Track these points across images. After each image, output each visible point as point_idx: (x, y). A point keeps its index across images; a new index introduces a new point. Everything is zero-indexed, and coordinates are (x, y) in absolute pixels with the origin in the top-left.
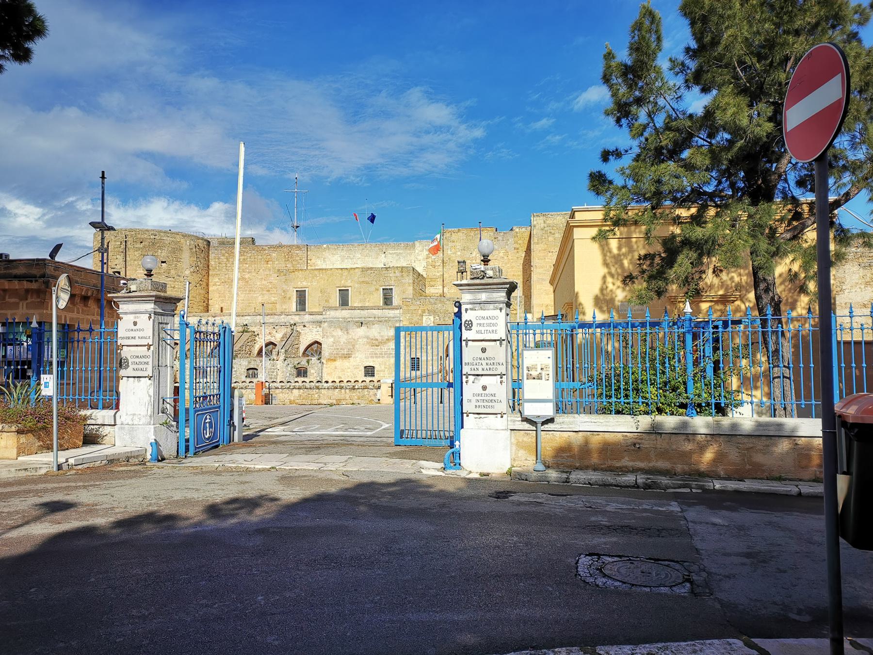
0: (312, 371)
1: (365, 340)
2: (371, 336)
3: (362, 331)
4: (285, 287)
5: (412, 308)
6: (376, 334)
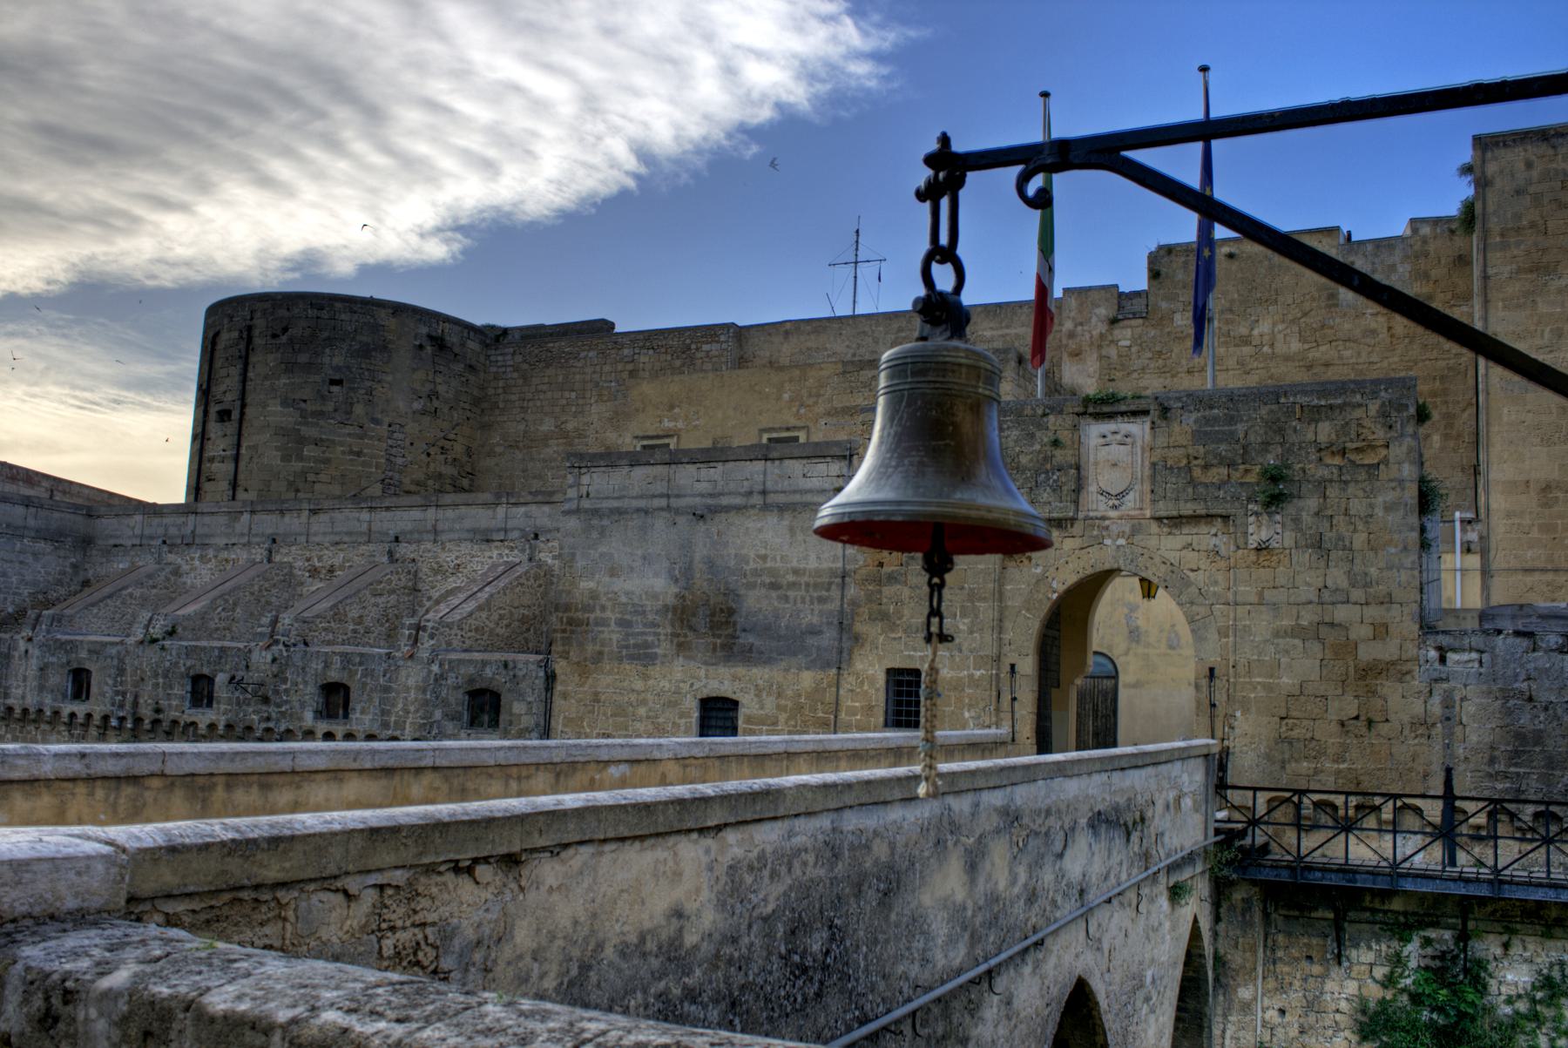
0: (518, 708)
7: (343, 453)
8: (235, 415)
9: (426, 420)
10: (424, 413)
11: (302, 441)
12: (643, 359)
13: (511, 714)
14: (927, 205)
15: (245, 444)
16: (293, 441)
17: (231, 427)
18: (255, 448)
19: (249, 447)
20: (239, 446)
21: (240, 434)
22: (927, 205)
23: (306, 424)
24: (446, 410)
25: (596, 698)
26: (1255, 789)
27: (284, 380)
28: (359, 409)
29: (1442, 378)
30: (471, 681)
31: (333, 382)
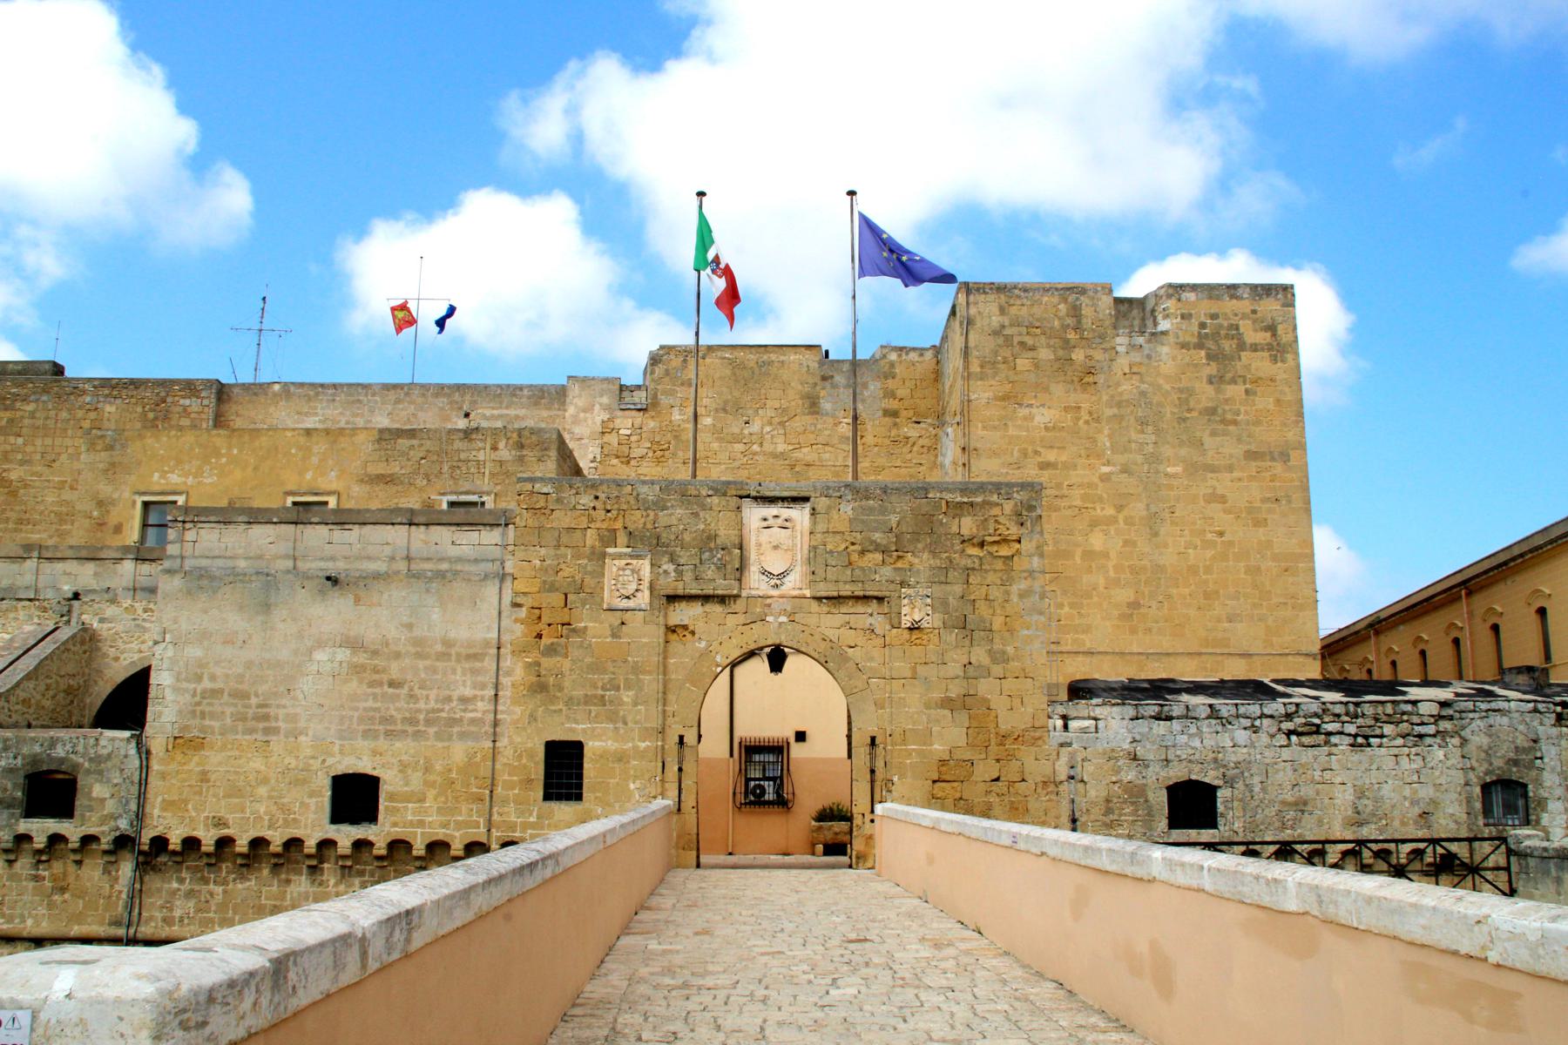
0: (99, 790)
1: (343, 654)
2: (371, 635)
3: (333, 613)
4: (105, 489)
5: (562, 519)
6: (392, 632)
12: (109, 408)
13: (91, 799)
25: (204, 777)
30: (35, 759)
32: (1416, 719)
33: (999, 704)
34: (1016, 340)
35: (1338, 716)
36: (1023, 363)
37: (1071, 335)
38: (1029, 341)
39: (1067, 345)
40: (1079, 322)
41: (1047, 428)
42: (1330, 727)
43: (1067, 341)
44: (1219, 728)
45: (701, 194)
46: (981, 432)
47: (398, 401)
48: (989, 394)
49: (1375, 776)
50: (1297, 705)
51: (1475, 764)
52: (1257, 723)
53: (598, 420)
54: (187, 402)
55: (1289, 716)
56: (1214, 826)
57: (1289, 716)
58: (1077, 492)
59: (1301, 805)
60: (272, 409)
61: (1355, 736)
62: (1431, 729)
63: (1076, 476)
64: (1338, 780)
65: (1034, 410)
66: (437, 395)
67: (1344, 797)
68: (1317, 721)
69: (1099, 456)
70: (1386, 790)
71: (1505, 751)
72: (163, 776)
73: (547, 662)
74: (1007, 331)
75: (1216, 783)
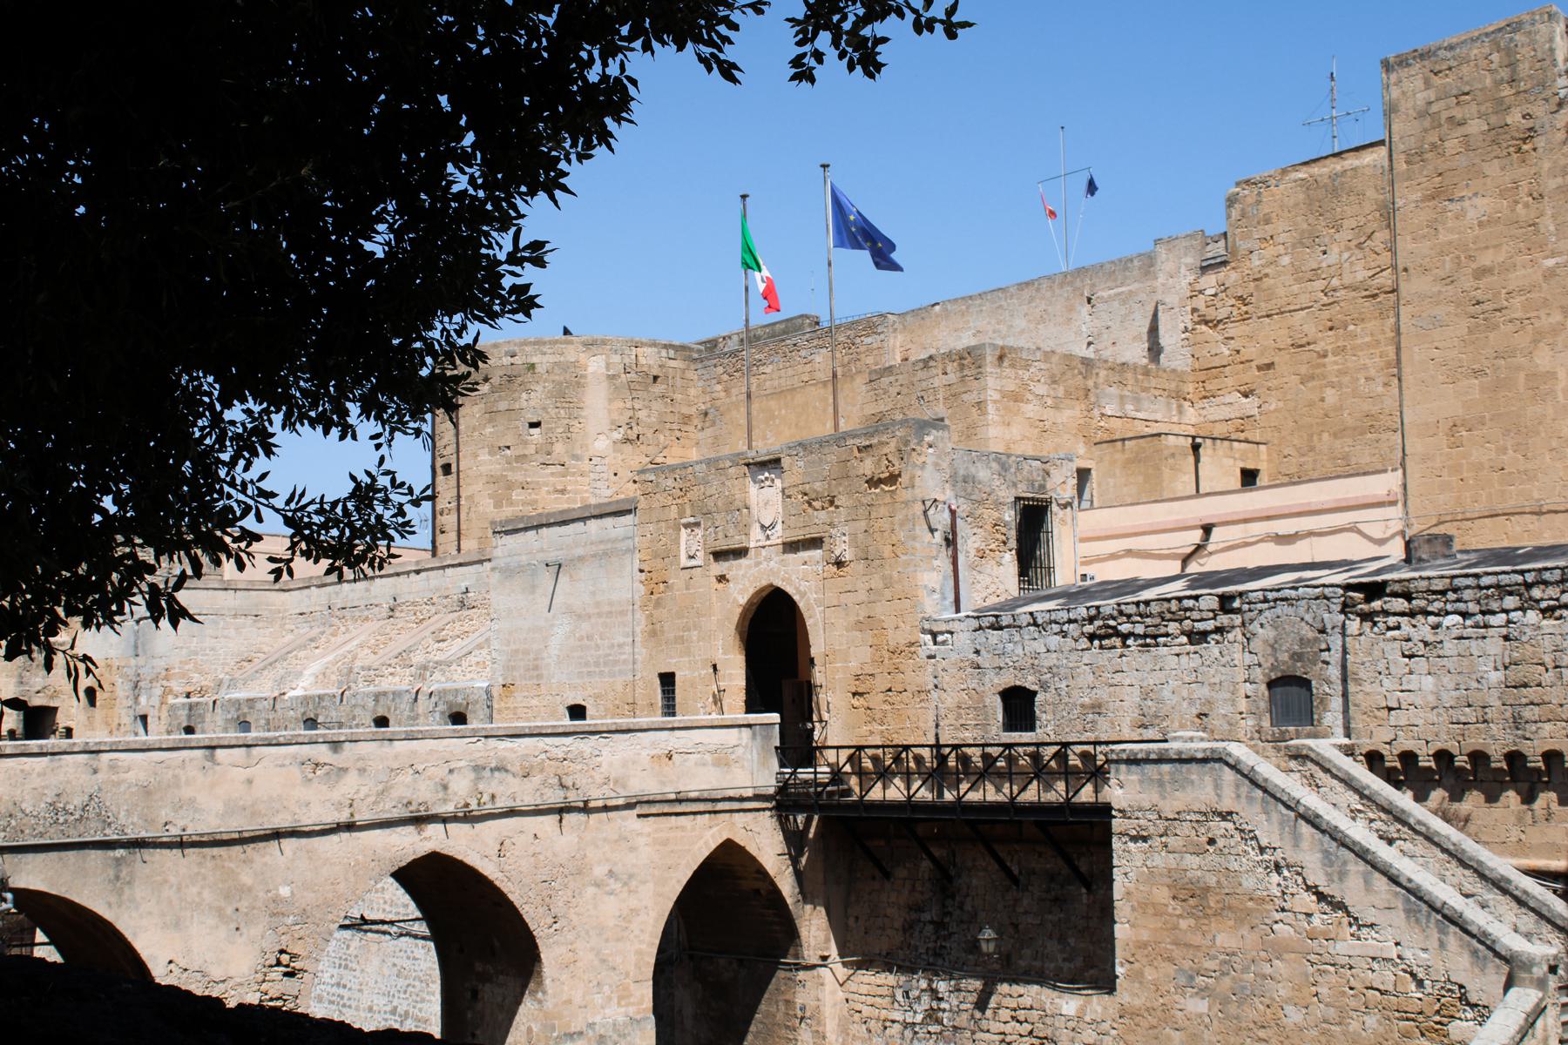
7: (549, 492)
8: (439, 471)
9: (628, 448)
10: (627, 440)
11: (510, 486)
14: (960, 31)
15: (463, 494)
16: (502, 487)
17: (452, 478)
18: (470, 497)
19: (467, 498)
20: (459, 497)
21: (458, 486)
22: (960, 31)
23: (512, 469)
24: (649, 434)
26: (838, 748)
27: (489, 430)
28: (559, 448)
29: (99, 815)
31: (534, 425)
32: (1195, 615)
33: (889, 623)
34: (1444, 115)
35: (1129, 616)
36: (1452, 145)
37: (1507, 91)
38: (1458, 113)
39: (1502, 107)
40: (1514, 71)
41: (1481, 224)
42: (1125, 628)
43: (1500, 101)
44: (1036, 635)
45: (744, 197)
46: (1411, 247)
47: (1032, 299)
48: (1418, 196)
49: (1158, 677)
50: (1098, 608)
51: (1262, 661)
52: (1065, 628)
53: (1184, 283)
54: (869, 340)
55: (1091, 620)
56: (1032, 728)
57: (1091, 620)
58: (1517, 301)
59: (1097, 708)
60: (936, 331)
61: (1145, 636)
62: (1210, 625)
63: (1517, 278)
64: (1128, 682)
65: (1467, 203)
66: (1061, 285)
67: (1132, 697)
68: (1112, 623)
69: (1542, 247)
70: (1166, 693)
71: (1290, 644)
72: (500, 711)
73: (656, 613)
74: (1434, 108)
75: (1034, 688)
